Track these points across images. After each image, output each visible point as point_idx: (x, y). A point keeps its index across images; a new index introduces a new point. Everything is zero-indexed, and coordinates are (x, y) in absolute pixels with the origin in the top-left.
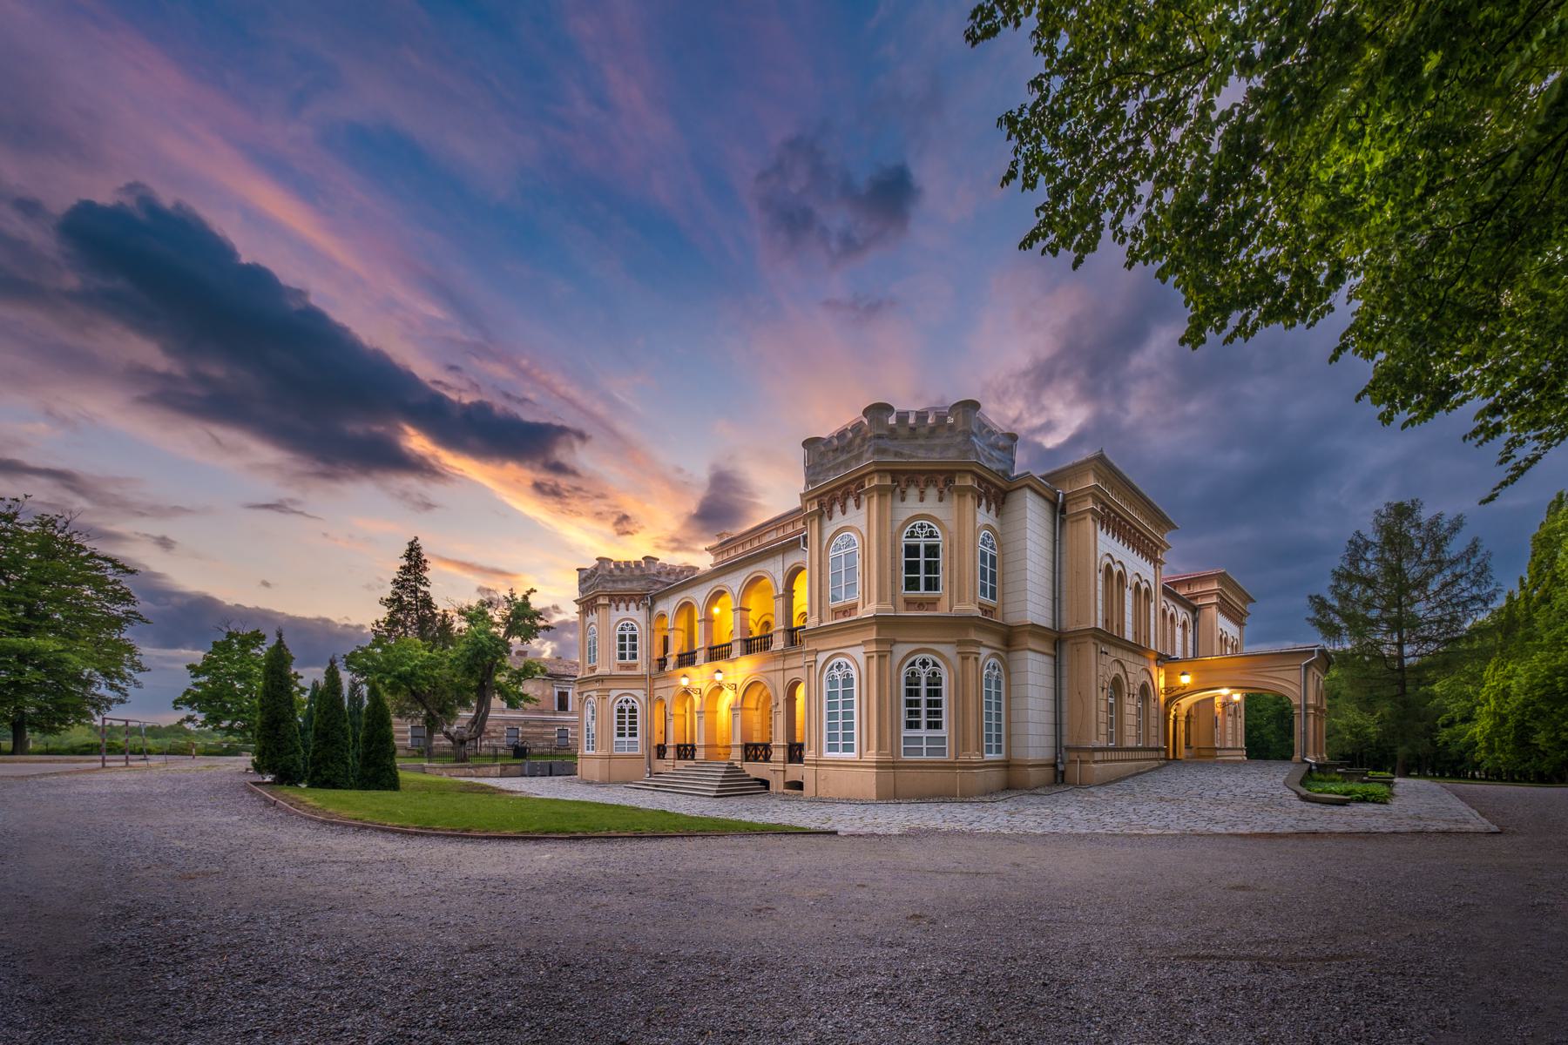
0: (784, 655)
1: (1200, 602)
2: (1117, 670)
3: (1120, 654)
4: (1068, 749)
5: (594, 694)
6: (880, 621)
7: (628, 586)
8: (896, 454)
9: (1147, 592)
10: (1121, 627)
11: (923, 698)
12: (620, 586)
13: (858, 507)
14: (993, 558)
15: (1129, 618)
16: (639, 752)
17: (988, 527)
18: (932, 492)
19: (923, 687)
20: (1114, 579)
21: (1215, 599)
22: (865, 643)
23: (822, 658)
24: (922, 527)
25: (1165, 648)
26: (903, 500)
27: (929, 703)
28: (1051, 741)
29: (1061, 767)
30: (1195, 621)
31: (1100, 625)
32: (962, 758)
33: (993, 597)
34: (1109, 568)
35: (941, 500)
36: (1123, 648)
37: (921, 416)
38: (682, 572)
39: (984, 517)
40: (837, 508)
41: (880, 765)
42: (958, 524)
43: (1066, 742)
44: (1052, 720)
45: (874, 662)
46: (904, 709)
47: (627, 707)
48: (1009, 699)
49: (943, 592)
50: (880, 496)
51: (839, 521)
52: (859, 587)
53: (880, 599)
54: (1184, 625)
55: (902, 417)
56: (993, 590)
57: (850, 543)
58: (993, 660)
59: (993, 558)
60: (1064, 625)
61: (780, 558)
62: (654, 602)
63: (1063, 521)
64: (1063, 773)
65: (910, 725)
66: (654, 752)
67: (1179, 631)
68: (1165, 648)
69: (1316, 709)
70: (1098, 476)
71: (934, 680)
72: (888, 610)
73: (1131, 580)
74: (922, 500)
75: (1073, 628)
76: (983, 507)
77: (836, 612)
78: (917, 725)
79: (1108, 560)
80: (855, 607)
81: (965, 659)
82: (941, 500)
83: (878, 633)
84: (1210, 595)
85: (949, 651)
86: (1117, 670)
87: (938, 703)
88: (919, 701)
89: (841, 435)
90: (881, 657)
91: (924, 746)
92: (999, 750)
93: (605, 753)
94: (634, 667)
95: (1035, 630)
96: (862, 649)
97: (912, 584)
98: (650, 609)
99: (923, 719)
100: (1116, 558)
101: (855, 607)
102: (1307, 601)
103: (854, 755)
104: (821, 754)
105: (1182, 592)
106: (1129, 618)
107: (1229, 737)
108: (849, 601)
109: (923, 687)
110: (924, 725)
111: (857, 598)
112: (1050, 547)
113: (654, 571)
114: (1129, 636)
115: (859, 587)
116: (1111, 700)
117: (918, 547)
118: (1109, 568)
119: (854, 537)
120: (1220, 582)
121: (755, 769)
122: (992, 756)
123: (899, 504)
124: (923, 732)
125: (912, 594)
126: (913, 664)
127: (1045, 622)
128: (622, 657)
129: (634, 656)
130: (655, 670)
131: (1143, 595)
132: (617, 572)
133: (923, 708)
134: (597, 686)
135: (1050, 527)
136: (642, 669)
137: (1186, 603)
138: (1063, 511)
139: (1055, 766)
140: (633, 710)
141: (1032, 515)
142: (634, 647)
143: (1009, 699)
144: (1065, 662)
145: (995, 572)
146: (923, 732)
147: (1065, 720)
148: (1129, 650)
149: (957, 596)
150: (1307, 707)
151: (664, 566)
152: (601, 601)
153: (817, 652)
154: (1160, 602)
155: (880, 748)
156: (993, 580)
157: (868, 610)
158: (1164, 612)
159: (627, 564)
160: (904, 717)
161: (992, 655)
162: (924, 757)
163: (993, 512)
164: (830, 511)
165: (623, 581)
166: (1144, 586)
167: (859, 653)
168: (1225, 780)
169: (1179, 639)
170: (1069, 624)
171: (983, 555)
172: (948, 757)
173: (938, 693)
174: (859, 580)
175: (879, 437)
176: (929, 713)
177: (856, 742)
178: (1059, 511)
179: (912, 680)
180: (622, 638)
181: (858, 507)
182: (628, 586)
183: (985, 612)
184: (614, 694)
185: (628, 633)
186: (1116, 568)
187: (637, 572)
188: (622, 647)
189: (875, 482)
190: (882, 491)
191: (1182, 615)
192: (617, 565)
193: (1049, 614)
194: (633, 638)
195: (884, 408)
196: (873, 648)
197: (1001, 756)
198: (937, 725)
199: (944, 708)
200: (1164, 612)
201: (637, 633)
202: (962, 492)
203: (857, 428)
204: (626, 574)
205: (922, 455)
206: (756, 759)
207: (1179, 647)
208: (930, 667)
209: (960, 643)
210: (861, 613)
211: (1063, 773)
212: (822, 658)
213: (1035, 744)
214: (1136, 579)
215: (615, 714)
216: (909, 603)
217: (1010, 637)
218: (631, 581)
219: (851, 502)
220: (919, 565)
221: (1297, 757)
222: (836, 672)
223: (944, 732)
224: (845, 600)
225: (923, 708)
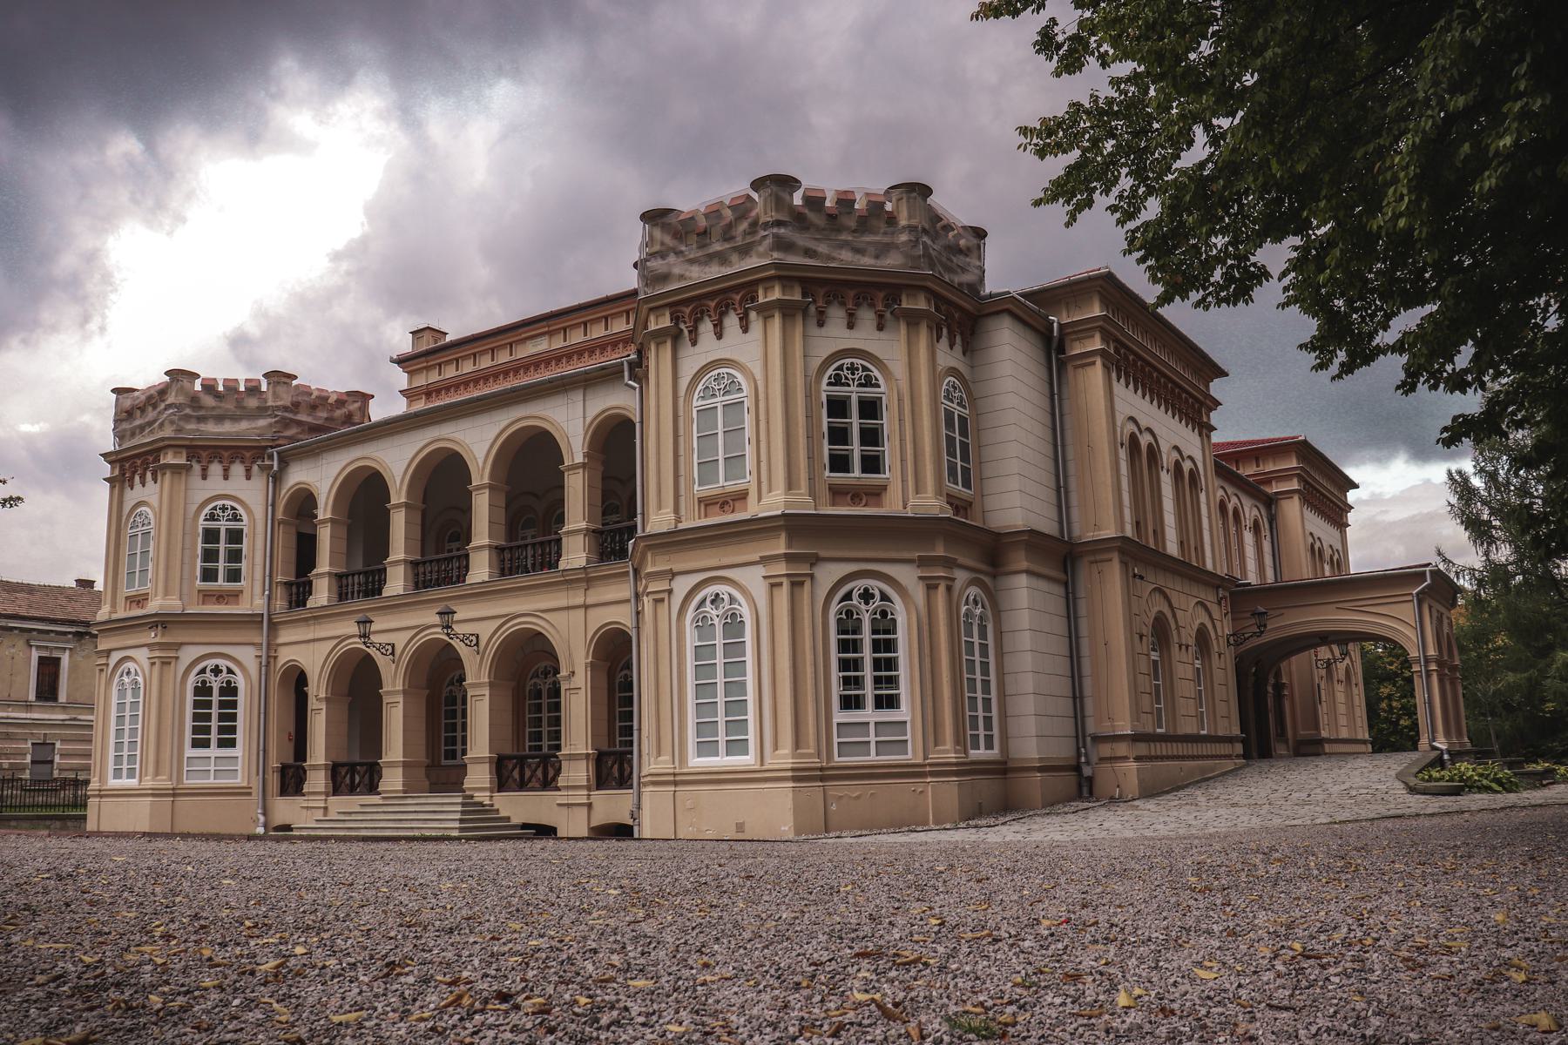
0: (585, 579)
1: (1275, 488)
2: (1159, 605)
3: (1162, 580)
4: (1097, 739)
5: (142, 655)
6: (792, 525)
7: (227, 428)
8: (809, 253)
9: (1194, 475)
10: (1159, 533)
11: (867, 654)
12: (211, 428)
13: (745, 329)
14: (963, 420)
15: (1170, 519)
16: (239, 780)
17: (953, 371)
18: (867, 317)
19: (867, 636)
20: (1142, 455)
21: (1294, 485)
22: (764, 560)
23: (682, 586)
24: (853, 369)
25: (1230, 566)
26: (821, 324)
27: (877, 665)
28: (1068, 727)
29: (1087, 771)
30: (1272, 519)
31: (1129, 532)
32: (934, 757)
33: (967, 484)
34: (1134, 440)
35: (880, 328)
36: (1166, 569)
37: (845, 201)
38: (340, 403)
39: (948, 357)
40: (706, 327)
41: (800, 776)
42: (903, 363)
43: (1091, 728)
44: (1068, 691)
45: (783, 594)
46: (835, 674)
47: (216, 684)
48: (1000, 654)
49: (891, 473)
50: (784, 316)
51: (707, 348)
52: (750, 463)
53: (790, 485)
54: (1256, 528)
55: (814, 201)
56: (966, 471)
57: (734, 387)
58: (973, 591)
59: (963, 420)
60: (1076, 532)
61: (577, 396)
62: (285, 462)
63: (1062, 365)
64: (1090, 780)
65: (196, 744)
66: (274, 781)
67: (1248, 537)
68: (1230, 566)
69: (1440, 663)
70: (1105, 303)
71: (884, 624)
72: (804, 504)
73: (1167, 458)
74: (719, 336)
75: (1090, 536)
76: (944, 340)
77: (707, 503)
78: (205, 744)
79: (1131, 427)
80: (742, 496)
81: (931, 587)
82: (880, 328)
83: (789, 546)
84: (1288, 478)
85: (907, 575)
86: (1159, 605)
87: (891, 664)
88: (861, 660)
89: (714, 213)
90: (796, 584)
91: (872, 738)
92: (989, 746)
93: (164, 782)
94: (235, 596)
95: (1033, 540)
96: (760, 571)
97: (840, 463)
98: (277, 479)
99: (869, 691)
100: (1143, 423)
101: (742, 496)
102: (1444, 477)
103: (747, 760)
104: (683, 759)
105: (1247, 470)
106: (1170, 519)
107: (1343, 721)
108: (732, 486)
109: (867, 636)
110: (870, 701)
111: (748, 481)
112: (1046, 404)
113: (286, 400)
114: (1172, 548)
115: (750, 463)
116: (1154, 656)
117: (218, 531)
118: (1134, 440)
119: (740, 377)
120: (1301, 458)
121: (518, 807)
122: (980, 753)
123: (814, 330)
124: (869, 714)
125: (839, 477)
126: (203, 671)
127: (1048, 526)
128: (209, 575)
129: (234, 576)
130: (280, 604)
131: (1186, 481)
132: (209, 401)
133: (868, 673)
134: (151, 637)
135: (1043, 373)
136: (253, 598)
137: (1252, 489)
138: (1061, 349)
139: (1077, 768)
140: (230, 690)
141: (1010, 356)
142: (235, 556)
143: (1000, 654)
144: (1081, 593)
145: (963, 443)
146: (869, 714)
147: (1088, 691)
148: (1175, 572)
149: (910, 490)
150: (1427, 661)
151: (306, 391)
152: (169, 458)
153: (673, 575)
154: (1212, 491)
155: (797, 744)
156: (965, 458)
157: (772, 502)
158: (1223, 506)
159: (231, 385)
160: (836, 690)
161: (972, 582)
162: (872, 757)
163: (958, 347)
164: (694, 332)
165: (220, 419)
166: (1187, 466)
167: (754, 579)
168: (1322, 777)
169: (1250, 551)
170: (1084, 532)
171: (949, 415)
172: (912, 755)
173: (890, 646)
174: (749, 451)
175: (779, 223)
176: (877, 680)
177: (752, 736)
178: (1055, 353)
179: (849, 624)
180: (211, 536)
181: (745, 329)
182: (227, 428)
183: (957, 510)
184: (188, 654)
185: (223, 525)
186: (1145, 440)
187: (252, 403)
188: (210, 556)
189: (776, 294)
190: (788, 311)
191: (1250, 511)
192: (209, 387)
193: (1052, 513)
194: (235, 536)
195: (787, 183)
196: (781, 569)
197: (995, 753)
198: (889, 702)
199: (903, 672)
200: (1223, 506)
201: (245, 525)
202: (912, 319)
203: (742, 207)
204: (229, 406)
205: (846, 257)
206: (522, 786)
207: (1251, 565)
208: (877, 602)
209: (923, 562)
210: (754, 509)
211: (1090, 780)
212: (682, 586)
213: (1034, 734)
214: (1175, 455)
215: (190, 697)
216: (837, 493)
217: (993, 552)
218: (235, 419)
219: (732, 322)
220: (848, 426)
221: (1424, 742)
222: (125, 678)
223: (904, 712)
224: (723, 483)
225: (868, 673)
